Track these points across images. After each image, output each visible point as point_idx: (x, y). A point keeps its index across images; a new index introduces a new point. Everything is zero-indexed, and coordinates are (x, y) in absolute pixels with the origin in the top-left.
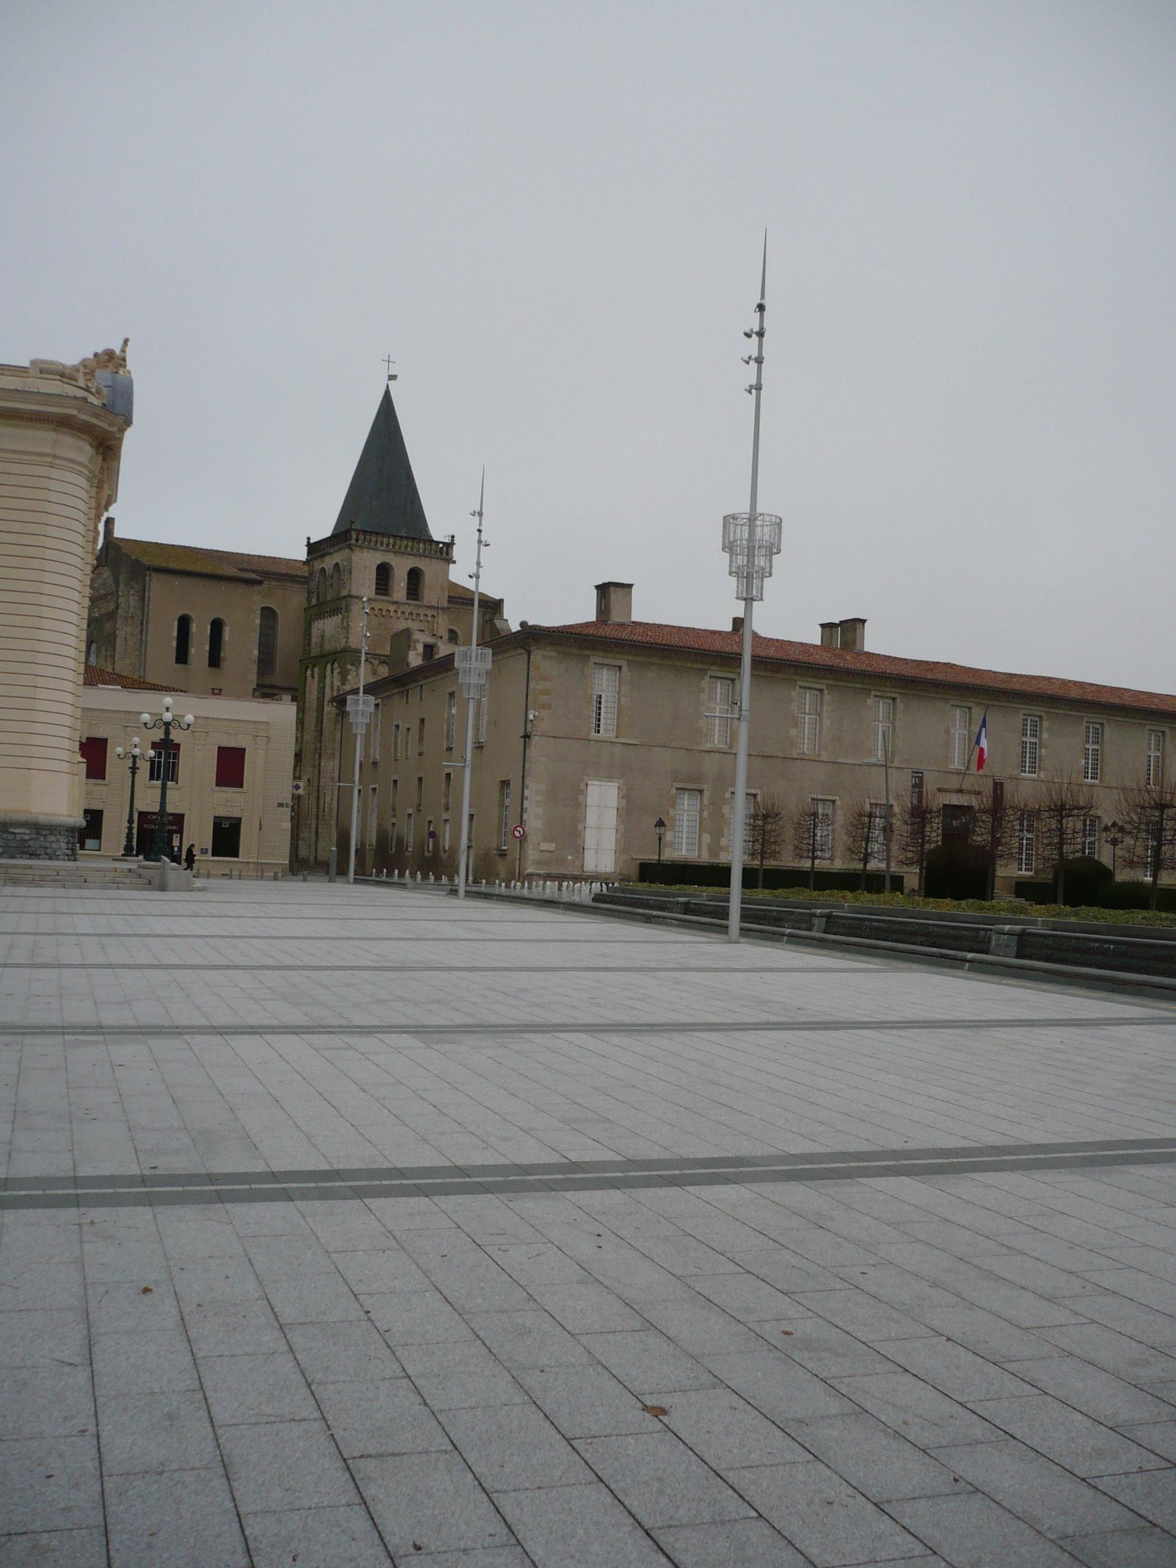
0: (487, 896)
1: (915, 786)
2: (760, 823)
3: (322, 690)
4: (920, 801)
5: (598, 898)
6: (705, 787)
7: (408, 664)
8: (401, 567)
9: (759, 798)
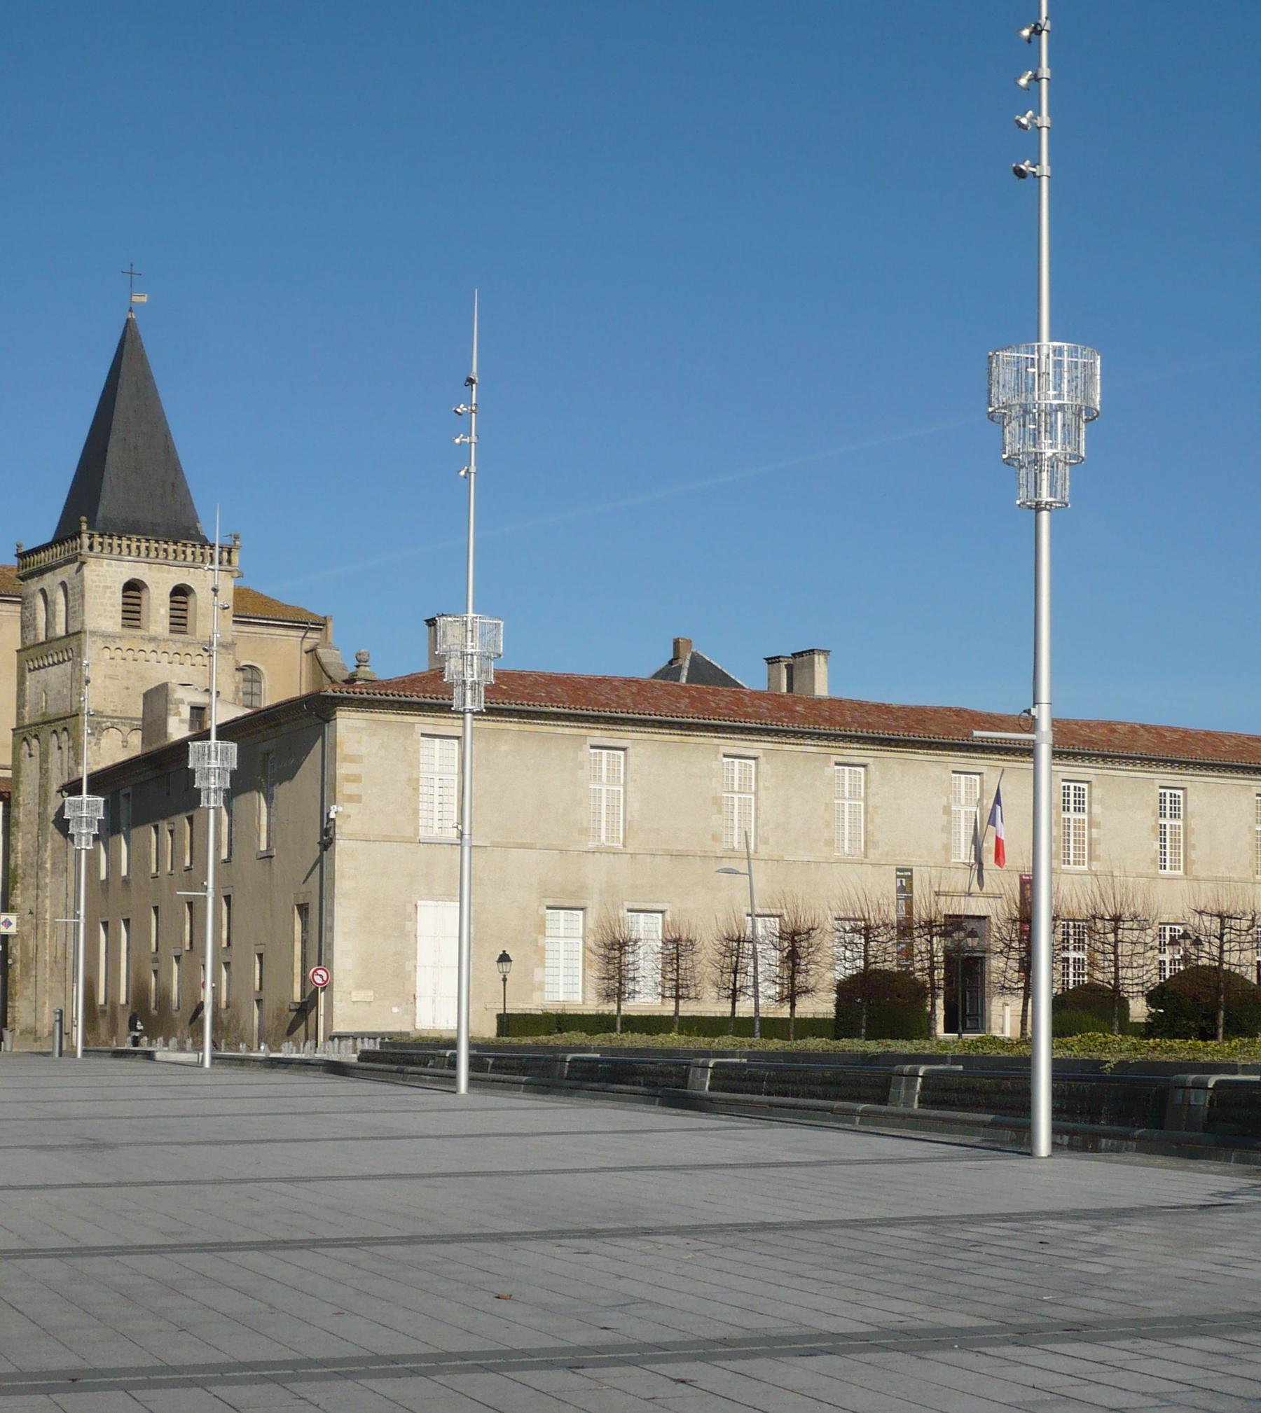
0: (242, 1062)
3: (44, 772)
5: (366, 1056)
6: (589, 903)
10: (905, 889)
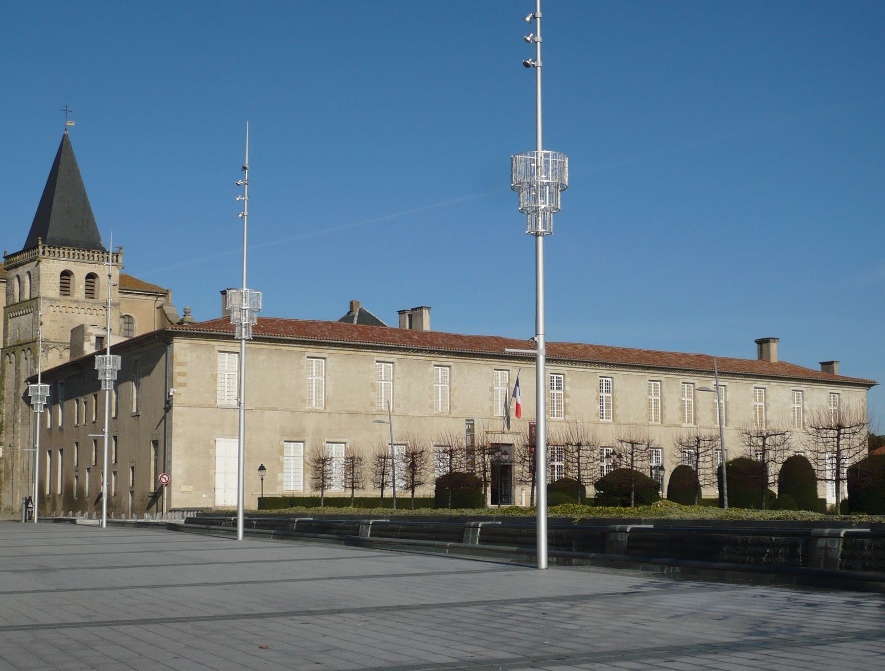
0: (123, 524)
1: (468, 430)
2: (321, 465)
3: (18, 371)
4: (473, 442)
6: (306, 439)
7: (83, 351)
8: (80, 271)
9: (348, 445)
10: (471, 430)
